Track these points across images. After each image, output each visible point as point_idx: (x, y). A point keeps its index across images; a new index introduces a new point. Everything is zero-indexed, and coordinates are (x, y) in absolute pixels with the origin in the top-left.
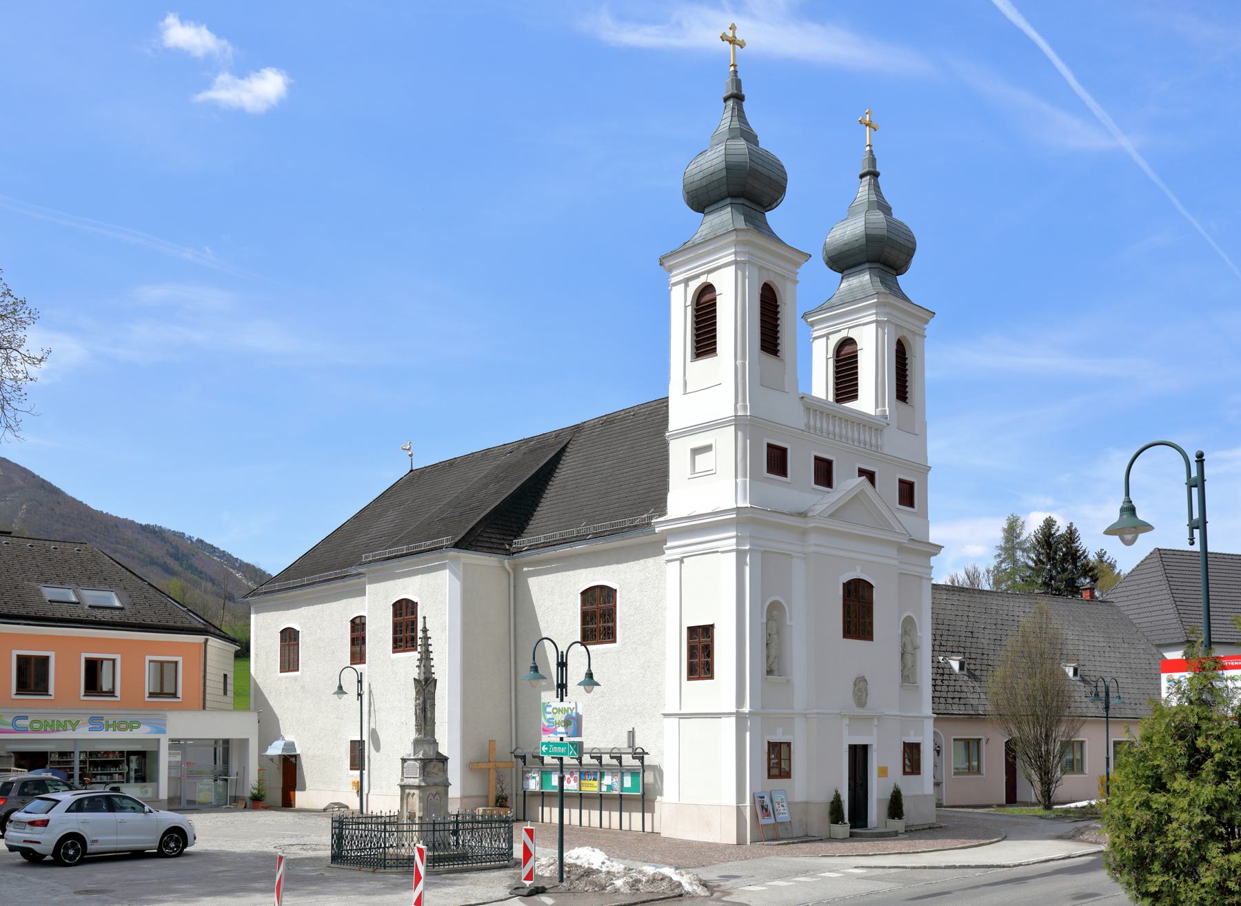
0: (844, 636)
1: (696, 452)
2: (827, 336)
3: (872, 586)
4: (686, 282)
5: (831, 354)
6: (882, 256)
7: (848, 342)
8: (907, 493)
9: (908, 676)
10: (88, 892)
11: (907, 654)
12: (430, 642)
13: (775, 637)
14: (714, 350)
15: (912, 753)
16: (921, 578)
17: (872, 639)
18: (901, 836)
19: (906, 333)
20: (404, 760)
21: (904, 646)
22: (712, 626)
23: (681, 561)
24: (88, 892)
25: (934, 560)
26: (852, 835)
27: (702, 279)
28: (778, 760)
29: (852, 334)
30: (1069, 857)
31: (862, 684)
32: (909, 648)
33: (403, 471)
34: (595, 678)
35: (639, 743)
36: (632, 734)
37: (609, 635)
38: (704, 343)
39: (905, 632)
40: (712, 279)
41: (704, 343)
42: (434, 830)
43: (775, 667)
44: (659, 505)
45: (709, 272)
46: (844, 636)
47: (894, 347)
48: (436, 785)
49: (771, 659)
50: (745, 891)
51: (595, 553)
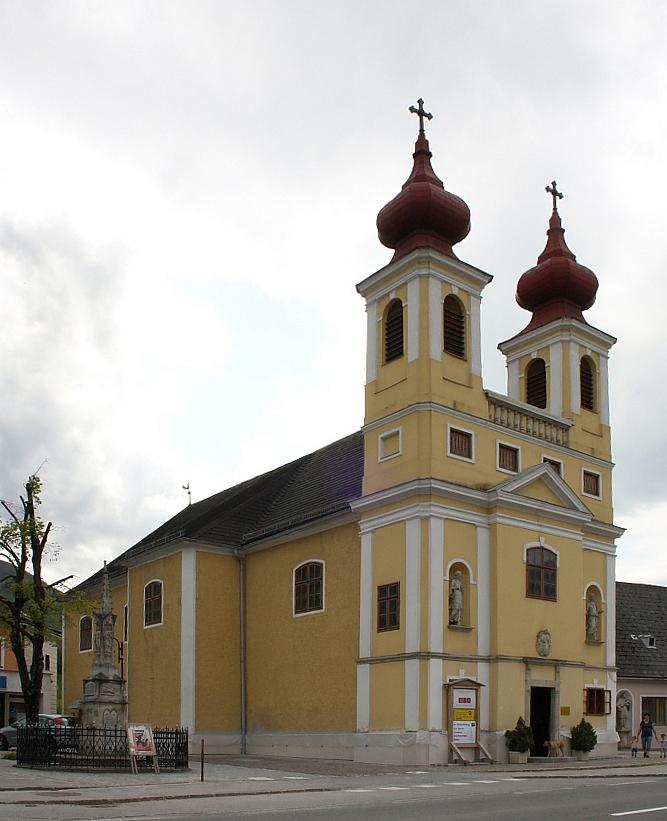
0: (528, 596)
8: (593, 483)
9: (593, 639)
11: (592, 617)
13: (458, 593)
14: (402, 354)
15: (595, 701)
16: (605, 554)
18: (474, 371)
19: (589, 353)
20: (86, 681)
21: (589, 610)
26: (529, 761)
31: (544, 637)
32: (594, 611)
33: (184, 506)
36: (32, 487)
37: (316, 604)
39: (590, 599)
44: (356, 491)
46: (528, 596)
48: (111, 703)
49: (454, 613)
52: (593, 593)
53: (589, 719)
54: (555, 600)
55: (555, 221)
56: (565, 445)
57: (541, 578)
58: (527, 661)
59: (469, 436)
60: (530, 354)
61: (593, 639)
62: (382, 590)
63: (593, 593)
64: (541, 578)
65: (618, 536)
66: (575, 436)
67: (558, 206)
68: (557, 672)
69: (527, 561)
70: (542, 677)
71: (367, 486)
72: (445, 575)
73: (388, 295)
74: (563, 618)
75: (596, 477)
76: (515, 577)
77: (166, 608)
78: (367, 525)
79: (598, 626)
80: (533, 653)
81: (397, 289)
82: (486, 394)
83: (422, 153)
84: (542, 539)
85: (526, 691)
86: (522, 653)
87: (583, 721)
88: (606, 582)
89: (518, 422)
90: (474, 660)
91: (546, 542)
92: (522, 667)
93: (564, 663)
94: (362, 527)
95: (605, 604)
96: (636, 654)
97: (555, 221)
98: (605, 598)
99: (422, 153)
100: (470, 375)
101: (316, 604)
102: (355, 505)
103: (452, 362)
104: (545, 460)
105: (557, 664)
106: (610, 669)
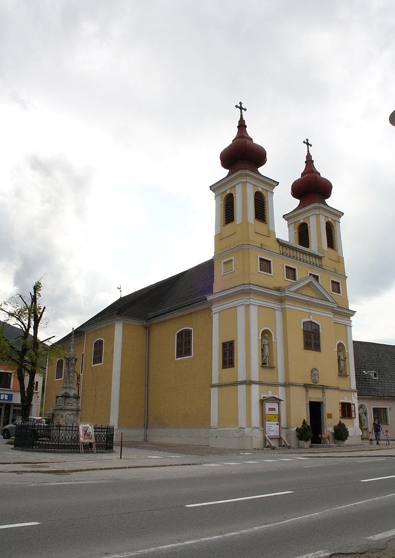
0: (305, 348)
2: (295, 223)
9: (342, 373)
11: (341, 360)
14: (233, 220)
15: (346, 410)
16: (346, 325)
19: (330, 220)
21: (339, 357)
22: (233, 341)
25: (352, 318)
26: (311, 447)
31: (315, 372)
32: (342, 358)
33: (117, 298)
35: (41, 302)
37: (188, 352)
39: (339, 350)
42: (60, 430)
43: (267, 361)
44: (210, 290)
46: (305, 348)
49: (264, 358)
50: (292, 491)
51: (183, 316)
52: (341, 347)
56: (321, 266)
57: (312, 339)
58: (306, 386)
61: (342, 373)
63: (341, 347)
64: (312, 339)
65: (352, 315)
66: (325, 262)
69: (304, 329)
70: (315, 396)
71: (217, 287)
74: (324, 361)
75: (338, 284)
76: (298, 339)
78: (215, 309)
80: (309, 381)
81: (231, 188)
82: (278, 240)
83: (242, 126)
84: (311, 317)
87: (340, 422)
90: (276, 385)
91: (347, 399)
93: (327, 387)
98: (347, 350)
99: (242, 126)
100: (269, 231)
101: (188, 352)
102: (209, 298)
103: (260, 225)
104: (310, 274)
105: (323, 388)
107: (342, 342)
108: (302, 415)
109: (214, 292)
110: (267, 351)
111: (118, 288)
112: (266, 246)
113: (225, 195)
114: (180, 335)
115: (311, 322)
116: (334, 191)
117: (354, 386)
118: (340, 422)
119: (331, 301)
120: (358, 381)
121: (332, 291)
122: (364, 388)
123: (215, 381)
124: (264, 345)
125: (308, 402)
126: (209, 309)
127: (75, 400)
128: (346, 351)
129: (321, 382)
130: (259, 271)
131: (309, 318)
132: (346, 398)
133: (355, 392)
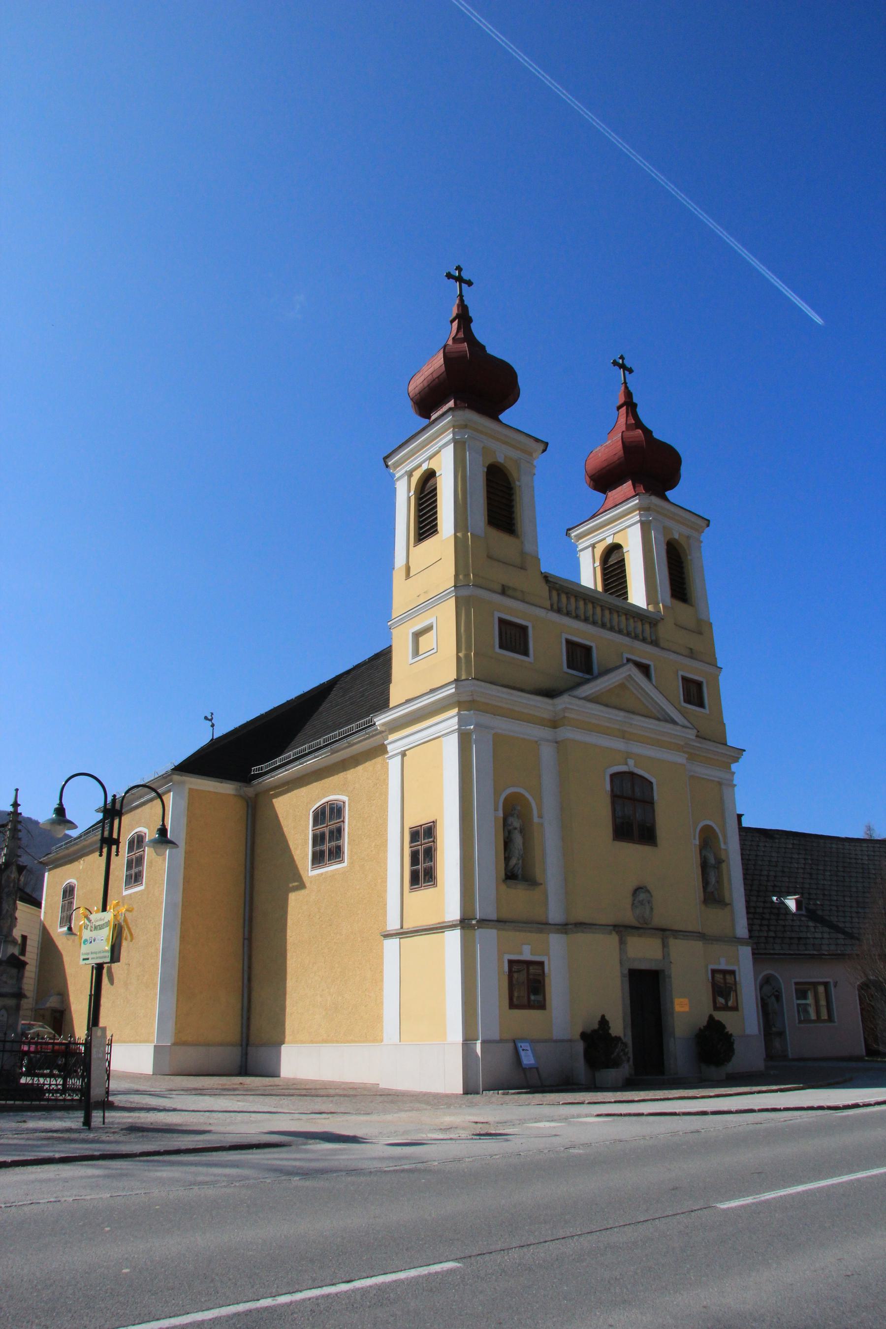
0: (614, 840)
1: (417, 635)
2: (593, 546)
3: (651, 783)
4: (410, 474)
5: (597, 563)
6: (645, 467)
7: (615, 548)
9: (713, 897)
10: (556, 1135)
11: (710, 866)
12: (20, 835)
15: (723, 987)
17: (656, 846)
18: (528, 548)
23: (403, 754)
24: (556, 1135)
25: (734, 767)
27: (425, 467)
28: (526, 985)
29: (618, 540)
30: (432, 691)
31: (642, 896)
32: (712, 860)
34: (69, 816)
37: (336, 854)
38: (425, 526)
40: (433, 465)
41: (425, 526)
44: (383, 704)
45: (430, 458)
46: (614, 840)
47: (663, 548)
52: (708, 840)
53: (719, 1016)
54: (656, 846)
55: (463, 309)
56: (655, 643)
57: (633, 814)
58: (621, 930)
59: (527, 627)
60: (604, 539)
61: (713, 897)
62: (415, 835)
63: (708, 840)
64: (633, 814)
65: (736, 760)
66: (665, 631)
67: (463, 294)
68: (665, 945)
69: (612, 790)
70: (645, 951)
71: (396, 694)
72: (496, 810)
73: (419, 466)
74: (669, 866)
75: (699, 685)
76: (599, 811)
77: (150, 866)
78: (395, 743)
79: (719, 881)
80: (628, 917)
81: (430, 458)
82: (546, 578)
83: (464, 318)
84: (631, 762)
85: (623, 975)
86: (610, 919)
87: (711, 1017)
88: (723, 817)
89: (590, 612)
90: (542, 926)
91: (635, 766)
92: (614, 939)
93: (676, 933)
94: (389, 748)
95: (726, 850)
96: (781, 922)
97: (463, 309)
98: (725, 843)
99: (464, 318)
100: (523, 554)
101: (336, 854)
102: (381, 720)
103: (500, 538)
104: (628, 660)
105: (665, 933)
106: (740, 941)
107: (708, 822)
108: (613, 1006)
109: (391, 706)
110: (518, 839)
111: (206, 718)
112: (515, 590)
113: (417, 475)
114: (320, 816)
115: (632, 774)
116: (685, 470)
117: (742, 930)
118: (711, 1017)
119: (680, 723)
120: (751, 916)
121: (685, 701)
122: (769, 934)
123: (393, 924)
124: (509, 832)
125: (626, 972)
126: (381, 750)
127: (14, 971)
128: (723, 846)
129: (658, 920)
130: (498, 650)
131: (627, 764)
132: (723, 960)
133: (747, 944)
